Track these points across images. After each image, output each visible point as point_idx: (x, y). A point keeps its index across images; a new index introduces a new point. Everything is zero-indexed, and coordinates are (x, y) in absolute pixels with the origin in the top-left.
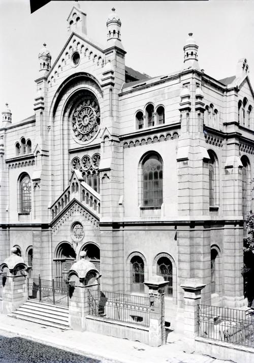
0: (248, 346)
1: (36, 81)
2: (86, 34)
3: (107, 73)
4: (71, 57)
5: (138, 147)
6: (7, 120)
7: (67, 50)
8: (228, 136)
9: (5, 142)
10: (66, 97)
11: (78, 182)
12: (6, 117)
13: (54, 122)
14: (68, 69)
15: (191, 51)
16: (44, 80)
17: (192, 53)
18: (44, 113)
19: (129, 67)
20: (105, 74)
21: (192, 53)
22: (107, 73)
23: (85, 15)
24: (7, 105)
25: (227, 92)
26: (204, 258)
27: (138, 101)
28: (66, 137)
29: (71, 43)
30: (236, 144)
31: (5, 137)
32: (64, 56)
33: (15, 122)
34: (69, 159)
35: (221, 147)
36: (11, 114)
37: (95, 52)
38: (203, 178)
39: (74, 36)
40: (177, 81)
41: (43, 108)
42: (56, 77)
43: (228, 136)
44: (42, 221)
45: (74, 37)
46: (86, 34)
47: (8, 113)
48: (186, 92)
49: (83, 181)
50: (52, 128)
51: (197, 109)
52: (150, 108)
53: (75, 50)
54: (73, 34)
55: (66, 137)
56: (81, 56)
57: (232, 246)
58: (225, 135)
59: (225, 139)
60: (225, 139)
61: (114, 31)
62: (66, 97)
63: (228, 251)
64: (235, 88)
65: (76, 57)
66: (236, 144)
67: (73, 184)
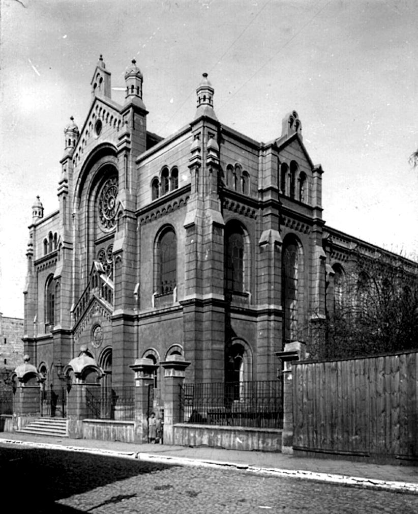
0: (223, 425)
1: (61, 162)
3: (123, 137)
4: (94, 126)
5: (154, 222)
7: (91, 119)
8: (263, 205)
9: (35, 241)
10: (90, 177)
11: (98, 274)
12: (36, 212)
13: (79, 209)
14: (92, 141)
16: (68, 160)
17: (205, 96)
18: (67, 198)
20: (120, 139)
21: (205, 96)
22: (123, 137)
23: (109, 74)
24: (38, 197)
25: (263, 151)
26: (212, 345)
29: (94, 111)
30: (353, 261)
31: (35, 236)
32: (87, 127)
34: (94, 252)
35: (253, 219)
37: (112, 112)
39: (97, 101)
41: (67, 193)
42: (80, 154)
43: (263, 205)
44: (62, 327)
45: (98, 103)
47: (39, 207)
49: (104, 273)
50: (76, 217)
51: (208, 165)
52: (165, 171)
53: (98, 118)
54: (96, 99)
55: (91, 226)
56: (104, 123)
59: (260, 209)
60: (260, 209)
61: (133, 87)
62: (90, 177)
63: (261, 349)
64: (272, 145)
65: (99, 126)
66: (353, 261)
67: (93, 277)
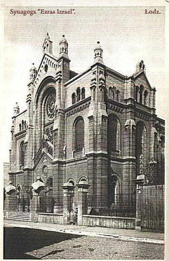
1: (28, 85)
2: (78, 74)
6: (16, 112)
7: (43, 64)
13: (37, 108)
15: (99, 52)
16: (31, 84)
17: (98, 53)
19: (72, 71)
21: (98, 53)
27: (72, 89)
28: (43, 116)
29: (44, 60)
33: (20, 112)
36: (19, 109)
38: (83, 190)
40: (90, 72)
42: (37, 82)
46: (78, 74)
48: (94, 77)
51: (100, 87)
53: (46, 64)
54: (45, 54)
55: (43, 116)
57: (127, 175)
58: (37, 94)
65: (46, 67)
